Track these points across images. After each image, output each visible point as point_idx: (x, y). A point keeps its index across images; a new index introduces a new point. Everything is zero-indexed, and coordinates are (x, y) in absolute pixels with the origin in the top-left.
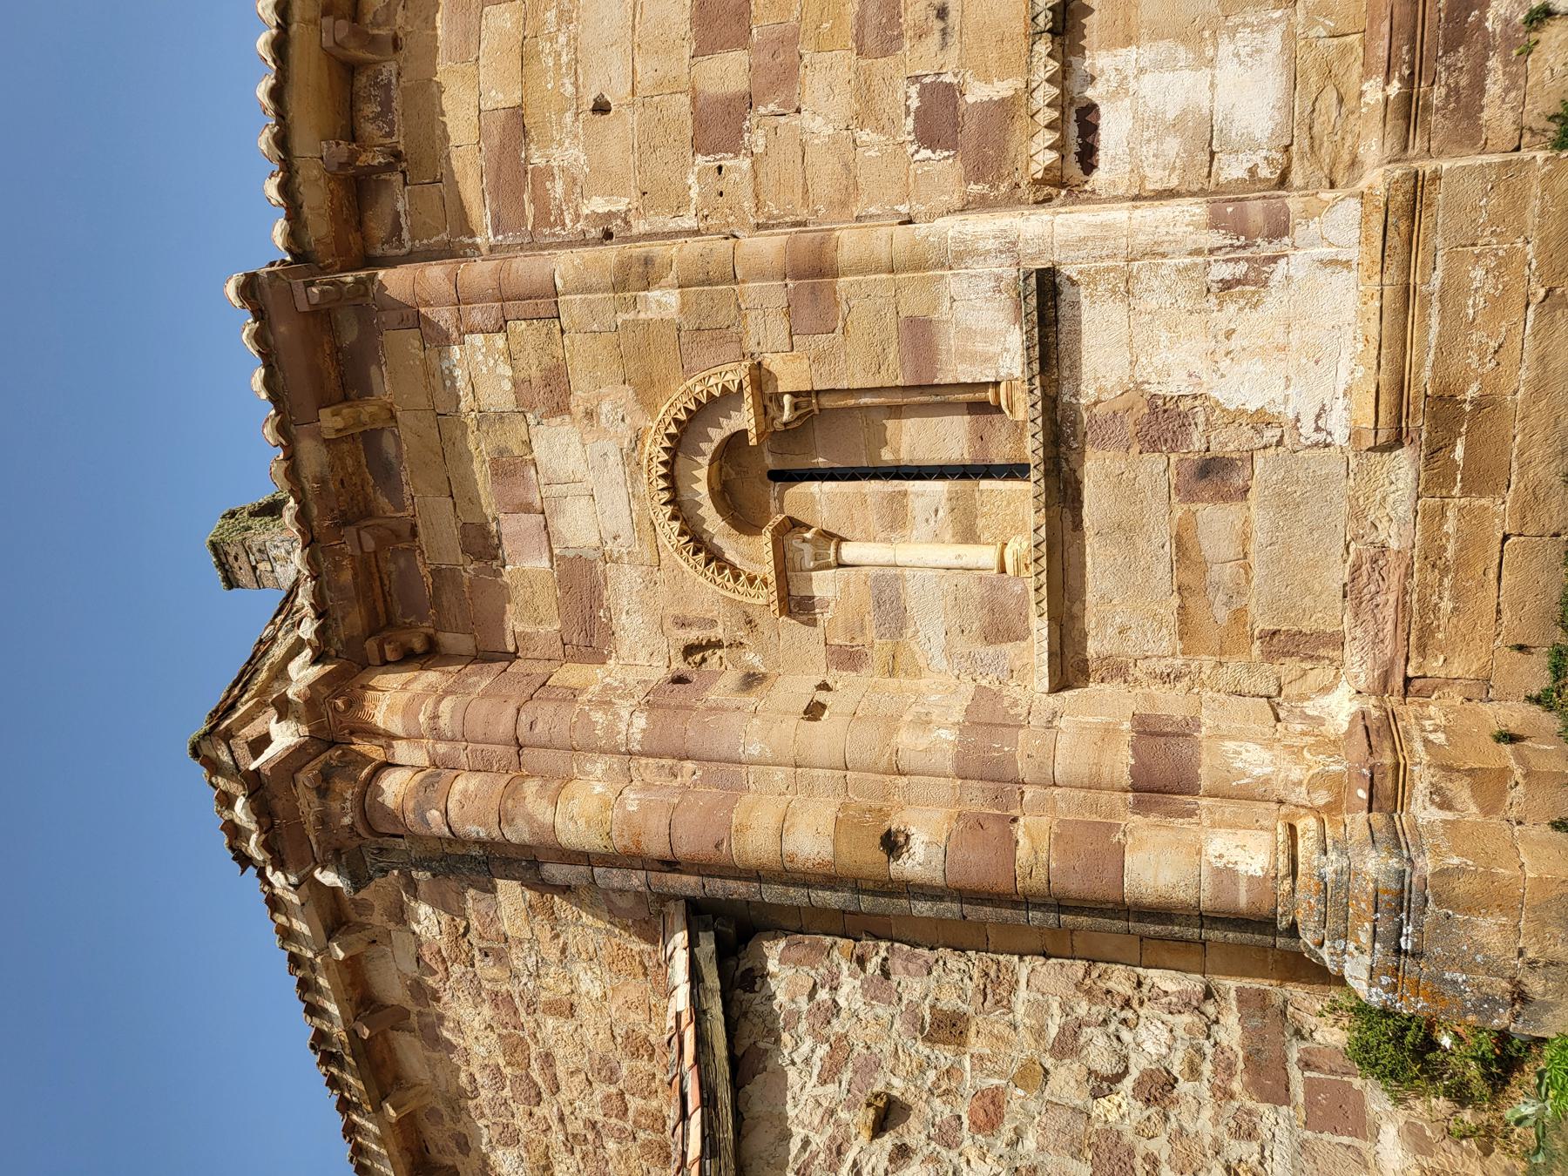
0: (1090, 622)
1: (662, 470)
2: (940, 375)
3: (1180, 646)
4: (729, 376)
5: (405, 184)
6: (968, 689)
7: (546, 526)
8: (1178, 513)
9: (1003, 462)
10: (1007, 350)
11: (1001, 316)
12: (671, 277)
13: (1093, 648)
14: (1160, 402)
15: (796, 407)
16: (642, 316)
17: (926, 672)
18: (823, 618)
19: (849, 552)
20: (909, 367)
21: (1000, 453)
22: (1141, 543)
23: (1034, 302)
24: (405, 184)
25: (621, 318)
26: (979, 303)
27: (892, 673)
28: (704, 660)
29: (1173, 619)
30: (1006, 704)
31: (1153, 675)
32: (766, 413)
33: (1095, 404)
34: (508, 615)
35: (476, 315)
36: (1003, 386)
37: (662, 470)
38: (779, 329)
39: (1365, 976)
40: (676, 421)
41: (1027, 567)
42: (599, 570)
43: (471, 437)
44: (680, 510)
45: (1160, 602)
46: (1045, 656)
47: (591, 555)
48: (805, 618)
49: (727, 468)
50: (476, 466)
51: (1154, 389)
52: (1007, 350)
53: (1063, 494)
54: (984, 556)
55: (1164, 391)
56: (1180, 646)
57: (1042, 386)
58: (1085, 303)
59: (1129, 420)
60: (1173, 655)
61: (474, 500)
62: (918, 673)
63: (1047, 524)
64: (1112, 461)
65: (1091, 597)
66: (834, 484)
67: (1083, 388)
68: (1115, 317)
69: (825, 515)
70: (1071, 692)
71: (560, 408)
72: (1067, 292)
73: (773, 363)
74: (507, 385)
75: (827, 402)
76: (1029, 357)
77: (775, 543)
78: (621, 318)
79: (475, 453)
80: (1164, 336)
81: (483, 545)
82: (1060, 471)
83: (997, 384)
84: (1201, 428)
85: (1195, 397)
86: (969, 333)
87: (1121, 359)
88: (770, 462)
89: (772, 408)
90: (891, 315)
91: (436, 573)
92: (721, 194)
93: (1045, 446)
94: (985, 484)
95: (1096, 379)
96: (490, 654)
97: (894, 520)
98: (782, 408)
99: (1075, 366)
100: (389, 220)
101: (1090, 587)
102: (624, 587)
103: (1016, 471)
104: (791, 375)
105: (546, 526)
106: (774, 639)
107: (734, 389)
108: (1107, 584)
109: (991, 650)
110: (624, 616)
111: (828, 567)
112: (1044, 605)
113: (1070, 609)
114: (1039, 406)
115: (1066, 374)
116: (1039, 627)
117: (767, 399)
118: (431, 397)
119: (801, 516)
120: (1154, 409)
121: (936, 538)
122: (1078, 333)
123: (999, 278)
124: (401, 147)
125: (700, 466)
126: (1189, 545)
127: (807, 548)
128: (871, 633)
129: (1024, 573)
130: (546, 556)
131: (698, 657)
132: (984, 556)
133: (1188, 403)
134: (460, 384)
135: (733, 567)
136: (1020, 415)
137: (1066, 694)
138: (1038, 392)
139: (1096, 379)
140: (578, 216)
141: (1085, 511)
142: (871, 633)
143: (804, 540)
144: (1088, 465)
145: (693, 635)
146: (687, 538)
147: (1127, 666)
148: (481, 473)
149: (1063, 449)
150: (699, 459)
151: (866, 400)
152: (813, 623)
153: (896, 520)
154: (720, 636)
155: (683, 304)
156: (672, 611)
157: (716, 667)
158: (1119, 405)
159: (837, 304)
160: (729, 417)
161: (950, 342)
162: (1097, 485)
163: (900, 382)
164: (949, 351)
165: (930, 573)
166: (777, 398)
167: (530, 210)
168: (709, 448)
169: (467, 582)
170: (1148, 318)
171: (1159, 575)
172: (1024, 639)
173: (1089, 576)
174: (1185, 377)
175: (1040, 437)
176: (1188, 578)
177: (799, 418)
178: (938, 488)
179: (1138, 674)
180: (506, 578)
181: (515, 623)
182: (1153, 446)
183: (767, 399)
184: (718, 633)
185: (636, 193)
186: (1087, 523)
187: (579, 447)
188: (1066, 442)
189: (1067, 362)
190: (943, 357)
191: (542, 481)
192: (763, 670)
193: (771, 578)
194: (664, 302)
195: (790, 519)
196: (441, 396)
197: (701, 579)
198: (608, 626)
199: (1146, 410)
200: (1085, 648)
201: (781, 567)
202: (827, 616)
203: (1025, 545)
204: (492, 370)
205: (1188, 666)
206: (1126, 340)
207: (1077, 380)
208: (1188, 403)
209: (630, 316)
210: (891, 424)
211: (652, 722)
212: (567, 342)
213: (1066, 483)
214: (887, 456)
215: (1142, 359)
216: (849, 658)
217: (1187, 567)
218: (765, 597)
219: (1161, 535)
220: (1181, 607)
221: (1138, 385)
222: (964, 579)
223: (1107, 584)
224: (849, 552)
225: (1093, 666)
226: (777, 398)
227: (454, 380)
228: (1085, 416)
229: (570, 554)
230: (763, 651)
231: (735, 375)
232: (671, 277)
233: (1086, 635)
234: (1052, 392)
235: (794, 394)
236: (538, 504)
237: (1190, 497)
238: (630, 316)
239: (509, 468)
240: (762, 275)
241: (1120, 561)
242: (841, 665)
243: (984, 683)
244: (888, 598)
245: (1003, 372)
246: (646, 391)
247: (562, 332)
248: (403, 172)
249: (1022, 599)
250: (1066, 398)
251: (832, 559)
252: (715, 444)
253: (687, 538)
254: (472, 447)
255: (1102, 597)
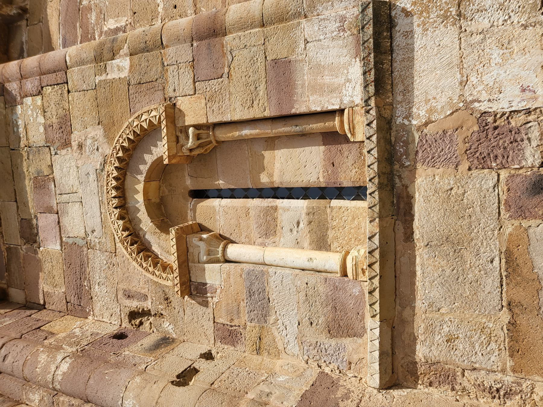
0: (420, 327)
1: (114, 183)
2: (296, 106)
3: (509, 363)
4: (154, 113)
5: (27, 26)
6: (312, 374)
7: (59, 222)
8: (509, 229)
9: (350, 185)
10: (349, 81)
11: (345, 51)
12: (125, 50)
13: (421, 352)
14: (490, 119)
15: (198, 137)
16: (109, 77)
17: (283, 355)
18: (213, 301)
19: (233, 251)
20: (274, 101)
21: (347, 178)
22: (469, 256)
23: (370, 30)
24: (27, 26)
25: (98, 79)
26: (326, 43)
27: (258, 351)
28: (141, 323)
29: (502, 334)
30: (339, 394)
31: (481, 387)
32: (178, 141)
33: (426, 124)
34: (40, 280)
35: (30, 85)
36: (346, 111)
37: (114, 183)
38: (187, 78)
39: (273, 58)
40: (123, 147)
41: (363, 271)
42: (85, 253)
43: (25, 164)
44: (127, 213)
45: (489, 316)
46: (377, 354)
47: (81, 242)
48: (200, 300)
49: (163, 188)
50: (27, 182)
51: (483, 107)
52: (349, 81)
53: (396, 208)
54: (330, 260)
55: (495, 107)
56: (509, 363)
57: (377, 106)
58: (418, 31)
59: (459, 138)
60: (503, 371)
61: (26, 204)
62: (278, 355)
63: (381, 233)
64: (442, 177)
65: (420, 305)
66: (229, 200)
67: (414, 110)
68: (446, 41)
69: (222, 223)
70: (404, 392)
71: (67, 144)
72: (401, 23)
73: (183, 103)
74: (42, 129)
75: (223, 135)
76: (365, 80)
77: (179, 239)
78: (98, 79)
79: (26, 173)
80: (496, 54)
81: (30, 235)
82: (393, 187)
83: (341, 111)
84: (534, 143)
85: (528, 112)
86: (318, 69)
87: (452, 80)
88: (189, 183)
89: (182, 137)
90: (261, 59)
91: (9, 249)
92: (175, 7)
93: (379, 160)
94: (335, 203)
95: (427, 101)
96: (32, 305)
97: (268, 229)
98: (187, 137)
99: (408, 91)
100: (19, 47)
101: (419, 295)
102: (97, 265)
103: (357, 193)
104: (194, 112)
105: (59, 222)
106: (182, 313)
107: (156, 123)
108: (435, 293)
109: (333, 342)
110: (97, 287)
111: (217, 261)
112: (377, 307)
113: (401, 313)
114: (374, 125)
115: (399, 98)
116: (373, 325)
117: (178, 132)
118: (8, 138)
119: (206, 224)
120: (484, 127)
121: (298, 244)
122: (411, 60)
123: (343, 19)
124: (28, 7)
125: (139, 182)
126: (520, 261)
127: (202, 244)
128: (244, 317)
129: (361, 277)
130: (59, 241)
131: (138, 321)
132: (330, 260)
133: (521, 118)
134: (21, 130)
135: (157, 256)
136: (360, 137)
137: (396, 393)
138: (373, 112)
139: (427, 101)
140: (101, 32)
141: (416, 224)
142: (244, 317)
143: (201, 239)
144: (419, 181)
145: (134, 304)
146: (127, 233)
147: (454, 375)
148: (28, 185)
149: (397, 167)
150: (139, 177)
151: (247, 132)
152: (205, 304)
153: (269, 229)
154: (150, 307)
155: (131, 66)
156: (121, 286)
157: (148, 329)
158: (449, 124)
159: (224, 55)
160: (156, 146)
161: (304, 77)
162: (427, 200)
163: (267, 114)
164: (303, 86)
165: (288, 271)
166: (185, 130)
167: (79, 32)
168: (144, 168)
169: (22, 256)
170: (479, 37)
171: (488, 289)
172: (361, 336)
173: (419, 284)
174: (517, 91)
175: (375, 152)
176: (520, 295)
177: (199, 146)
178: (300, 205)
179: (466, 384)
180: (40, 255)
181: (44, 286)
182: (483, 163)
183: (178, 132)
184: (148, 305)
185: (130, 13)
186: (417, 235)
187: (75, 169)
188: (399, 160)
189: (400, 87)
190: (299, 91)
191: (58, 192)
192: (174, 336)
193: (175, 266)
194: (121, 67)
195: (200, 225)
196: (12, 137)
197: (134, 263)
198: (89, 292)
199: (476, 128)
200: (414, 352)
201: (183, 258)
202: (215, 300)
203: (362, 252)
204: (35, 119)
205: (520, 384)
206: (456, 61)
207: (410, 103)
208: (521, 118)
209: (103, 77)
210: (267, 154)
211: (72, 367)
212: (70, 99)
213: (399, 197)
214: (264, 179)
215: (473, 79)
216: (229, 335)
217: (517, 284)
218: (171, 282)
219: (492, 248)
220: (512, 324)
221: (468, 105)
222: (313, 278)
223: (435, 293)
224: (233, 251)
225: (421, 369)
226: (185, 130)
227: (18, 127)
228: (417, 136)
229: (70, 241)
230: (174, 322)
231: (153, 111)
232: (125, 50)
233: (415, 339)
234: (387, 114)
235: (197, 127)
236: (55, 208)
237: (521, 212)
238: (103, 77)
239: (43, 182)
240: (178, 40)
241: (448, 271)
242: (224, 340)
243: (327, 370)
244: (257, 290)
245: (346, 100)
246: (109, 127)
247: (69, 92)
248: (27, 20)
249: (359, 300)
250: (399, 120)
251: (220, 255)
252: (148, 166)
253: (127, 233)
254: (25, 170)
255: (430, 305)
